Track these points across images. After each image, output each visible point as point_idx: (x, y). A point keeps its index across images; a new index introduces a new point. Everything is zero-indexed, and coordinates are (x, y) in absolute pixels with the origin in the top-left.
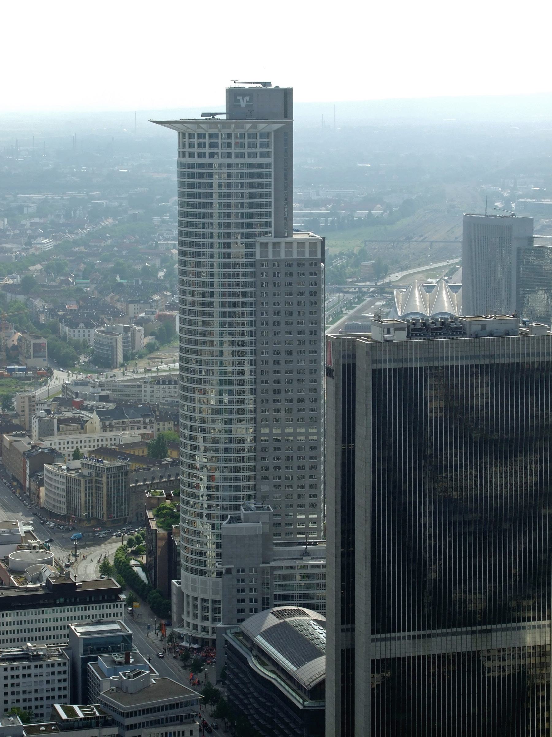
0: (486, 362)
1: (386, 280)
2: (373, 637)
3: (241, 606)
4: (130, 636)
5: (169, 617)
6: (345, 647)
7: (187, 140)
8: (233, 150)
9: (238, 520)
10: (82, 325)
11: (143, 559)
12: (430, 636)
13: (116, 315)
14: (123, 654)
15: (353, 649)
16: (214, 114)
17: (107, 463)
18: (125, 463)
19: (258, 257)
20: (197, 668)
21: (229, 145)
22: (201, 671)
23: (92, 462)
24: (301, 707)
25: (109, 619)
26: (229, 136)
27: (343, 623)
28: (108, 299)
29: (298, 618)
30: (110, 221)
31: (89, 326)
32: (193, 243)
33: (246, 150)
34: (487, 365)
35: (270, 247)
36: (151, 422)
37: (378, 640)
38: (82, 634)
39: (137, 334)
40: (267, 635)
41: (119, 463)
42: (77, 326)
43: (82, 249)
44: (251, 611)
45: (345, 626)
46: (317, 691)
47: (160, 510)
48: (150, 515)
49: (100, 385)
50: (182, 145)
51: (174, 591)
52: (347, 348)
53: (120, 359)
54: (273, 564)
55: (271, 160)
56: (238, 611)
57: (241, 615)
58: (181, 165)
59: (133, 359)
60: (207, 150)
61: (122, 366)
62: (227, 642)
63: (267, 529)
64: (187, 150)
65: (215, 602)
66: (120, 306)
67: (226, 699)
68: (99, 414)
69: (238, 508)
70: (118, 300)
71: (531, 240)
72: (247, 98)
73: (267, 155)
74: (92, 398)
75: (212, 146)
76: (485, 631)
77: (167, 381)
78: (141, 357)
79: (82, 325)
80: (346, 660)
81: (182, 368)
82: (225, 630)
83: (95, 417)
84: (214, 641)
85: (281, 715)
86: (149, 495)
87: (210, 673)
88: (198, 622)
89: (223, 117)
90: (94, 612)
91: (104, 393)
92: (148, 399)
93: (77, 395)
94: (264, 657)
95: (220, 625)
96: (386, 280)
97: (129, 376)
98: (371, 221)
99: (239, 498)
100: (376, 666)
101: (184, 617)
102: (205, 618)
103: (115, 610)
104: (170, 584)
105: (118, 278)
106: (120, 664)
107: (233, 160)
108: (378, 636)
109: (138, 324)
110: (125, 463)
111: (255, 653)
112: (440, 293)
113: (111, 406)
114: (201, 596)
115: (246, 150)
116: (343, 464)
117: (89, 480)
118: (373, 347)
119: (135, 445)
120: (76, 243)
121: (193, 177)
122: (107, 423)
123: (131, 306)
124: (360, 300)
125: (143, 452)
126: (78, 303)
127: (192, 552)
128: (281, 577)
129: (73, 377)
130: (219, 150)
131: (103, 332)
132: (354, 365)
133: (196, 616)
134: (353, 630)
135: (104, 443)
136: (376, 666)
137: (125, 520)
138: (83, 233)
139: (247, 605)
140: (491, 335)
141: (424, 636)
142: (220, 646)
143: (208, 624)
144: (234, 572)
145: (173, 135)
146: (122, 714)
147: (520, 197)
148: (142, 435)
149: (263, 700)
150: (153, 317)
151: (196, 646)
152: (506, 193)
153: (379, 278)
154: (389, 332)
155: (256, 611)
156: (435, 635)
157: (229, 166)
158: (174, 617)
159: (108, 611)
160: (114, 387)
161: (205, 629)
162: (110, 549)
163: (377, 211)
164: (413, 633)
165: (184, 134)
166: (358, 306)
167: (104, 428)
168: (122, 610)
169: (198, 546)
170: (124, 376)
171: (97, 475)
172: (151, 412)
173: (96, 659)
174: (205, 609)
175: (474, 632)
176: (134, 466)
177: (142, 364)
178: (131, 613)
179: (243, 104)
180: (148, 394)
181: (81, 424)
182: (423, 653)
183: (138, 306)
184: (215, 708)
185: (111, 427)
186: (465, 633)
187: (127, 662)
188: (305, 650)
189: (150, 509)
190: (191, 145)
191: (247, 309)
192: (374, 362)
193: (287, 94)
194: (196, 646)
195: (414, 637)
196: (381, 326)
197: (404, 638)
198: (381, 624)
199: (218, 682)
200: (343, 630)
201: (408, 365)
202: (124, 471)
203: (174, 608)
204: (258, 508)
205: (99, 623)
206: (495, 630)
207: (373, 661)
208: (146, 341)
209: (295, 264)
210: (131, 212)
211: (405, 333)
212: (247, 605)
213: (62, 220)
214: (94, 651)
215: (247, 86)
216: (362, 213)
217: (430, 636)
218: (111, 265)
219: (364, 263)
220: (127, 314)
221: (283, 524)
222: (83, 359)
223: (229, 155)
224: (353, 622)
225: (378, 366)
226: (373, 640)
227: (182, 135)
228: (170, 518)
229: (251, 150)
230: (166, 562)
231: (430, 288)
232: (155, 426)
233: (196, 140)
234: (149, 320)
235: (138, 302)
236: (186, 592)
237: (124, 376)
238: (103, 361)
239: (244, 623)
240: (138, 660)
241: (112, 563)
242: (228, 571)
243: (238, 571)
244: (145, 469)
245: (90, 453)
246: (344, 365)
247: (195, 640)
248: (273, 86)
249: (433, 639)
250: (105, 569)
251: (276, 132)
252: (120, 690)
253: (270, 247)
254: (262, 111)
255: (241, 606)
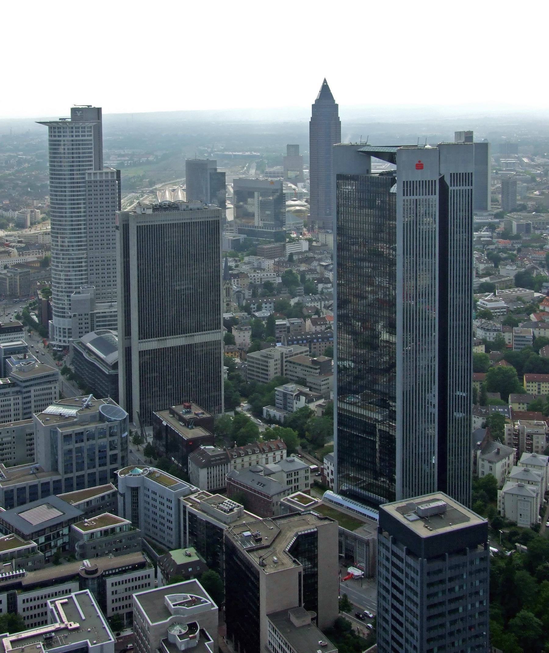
0: (188, 221)
1: (154, 187)
2: (140, 341)
3: (81, 330)
4: (27, 346)
5: (48, 337)
6: (127, 346)
7: (52, 130)
8: (74, 134)
9: (79, 293)
10: (11, 210)
11: (37, 312)
12: (193, 335)
13: (28, 206)
14: (23, 354)
15: (131, 347)
16: (65, 119)
17: (19, 270)
18: (28, 270)
19: (87, 179)
20: (60, 358)
21: (72, 132)
22: (62, 360)
23: (12, 270)
24: (107, 373)
25: (17, 339)
26: (72, 128)
27: (126, 335)
28: (24, 198)
29: (107, 334)
30: (27, 165)
31: (14, 210)
32: (55, 174)
33: (80, 134)
34: (189, 223)
35: (92, 175)
36: (42, 251)
37: (142, 342)
38: (3, 346)
39: (37, 213)
40: (91, 343)
41: (26, 270)
42: (8, 210)
43: (13, 177)
44: (86, 332)
45: (126, 337)
46: (115, 366)
47: (44, 290)
48: (39, 292)
49: (18, 236)
50: (50, 131)
51: (50, 325)
52: (126, 216)
53: (29, 224)
54: (95, 311)
55: (92, 138)
56: (80, 333)
57: (81, 334)
58: (50, 141)
59: (35, 224)
60: (57, 134)
61: (30, 227)
62: (74, 347)
63: (93, 296)
64: (53, 134)
65: (69, 329)
66: (30, 201)
67: (73, 372)
68: (17, 249)
69: (79, 288)
70: (29, 199)
71: (216, 169)
72: (81, 112)
73: (91, 135)
74: (14, 242)
75: (59, 132)
76: (191, 336)
77: (46, 234)
78: (39, 223)
79: (11, 210)
80: (128, 352)
81: (52, 228)
82: (73, 342)
83: (15, 250)
84: (68, 346)
85: (98, 377)
86: (38, 284)
87: (67, 360)
88: (62, 338)
89: (70, 120)
90: (10, 337)
91: (20, 240)
92: (41, 242)
93: (7, 241)
94: (90, 351)
95: (71, 339)
96: (154, 187)
97: (33, 231)
98: (148, 163)
99: (80, 283)
100: (142, 354)
101: (55, 336)
102: (65, 337)
103: (21, 335)
104: (48, 323)
105: (29, 190)
106: (21, 359)
107: (74, 138)
108: (142, 341)
109: (37, 209)
110: (28, 270)
111: (86, 351)
112: (178, 192)
113: (23, 245)
114: (62, 327)
115: (80, 134)
116: (124, 267)
117: (11, 278)
118: (137, 216)
119: (34, 262)
120: (10, 175)
121: (54, 145)
122: (21, 253)
123: (35, 201)
124: (142, 196)
125: (38, 265)
126: (10, 200)
127: (58, 308)
128: (99, 317)
129: (6, 233)
130: (68, 134)
131: (20, 213)
132: (128, 224)
133: (60, 336)
134: (130, 338)
135: (19, 261)
136: (142, 354)
137: (28, 295)
138: (12, 171)
139: (84, 330)
140: (191, 210)
141: (163, 339)
142: (71, 349)
143: (66, 339)
144: (77, 316)
145: (46, 128)
146: (21, 381)
147: (216, 151)
148: (38, 258)
149: (90, 371)
150: (45, 206)
151: (60, 349)
152: (209, 150)
153: (151, 187)
154: (144, 210)
155: (88, 332)
156: (168, 339)
157: (72, 141)
158: (50, 337)
159: (15, 336)
160: (25, 237)
161: (64, 341)
162: (19, 309)
163: (151, 158)
164: (158, 338)
165: (51, 128)
166: (141, 199)
167: (19, 255)
168: (24, 335)
169: (61, 306)
170: (27, 232)
171: (15, 275)
172: (44, 247)
173: (10, 357)
174: (64, 333)
175: (186, 336)
176: (32, 271)
177: (39, 226)
178: (30, 336)
179: (79, 115)
180: (41, 239)
181: (8, 253)
182: (188, 343)
183: (38, 201)
184: (68, 376)
185: (23, 255)
186: (182, 337)
187: (25, 357)
188: (108, 347)
189: (39, 289)
190: (55, 132)
191: (82, 201)
192: (137, 223)
193: (99, 110)
194: (60, 349)
195: (159, 340)
196: (141, 208)
197: (154, 341)
198: (144, 335)
199: (71, 364)
200: (126, 339)
201: (153, 224)
202: (28, 274)
203: (50, 333)
204: (88, 287)
205: (12, 341)
206: (195, 335)
207: (140, 352)
208: (41, 216)
209: (93, 182)
210: (37, 160)
211: (151, 210)
212: (84, 330)
213: (4, 165)
214: (9, 354)
215: (80, 107)
216: (144, 159)
217: (166, 339)
218: (26, 184)
219: (144, 180)
220: (33, 204)
221: (101, 294)
222: (11, 225)
223: (72, 136)
224: (130, 335)
225: (139, 225)
226: (139, 343)
227: (50, 128)
228: (47, 293)
229: (77, 134)
230: (47, 313)
231: (174, 190)
232: (44, 253)
233: (57, 130)
234: (43, 207)
235: (38, 200)
236: (55, 325)
237: (27, 232)
238: (21, 225)
239: (82, 338)
240: (30, 356)
241: (21, 314)
242: (75, 316)
243: (79, 315)
244: (38, 272)
245: (12, 266)
246: (123, 225)
247: (60, 347)
248: (93, 107)
249: (168, 341)
250: (18, 317)
251: (94, 126)
252: (21, 370)
253: (92, 175)
254: (87, 118)
255: (81, 330)
